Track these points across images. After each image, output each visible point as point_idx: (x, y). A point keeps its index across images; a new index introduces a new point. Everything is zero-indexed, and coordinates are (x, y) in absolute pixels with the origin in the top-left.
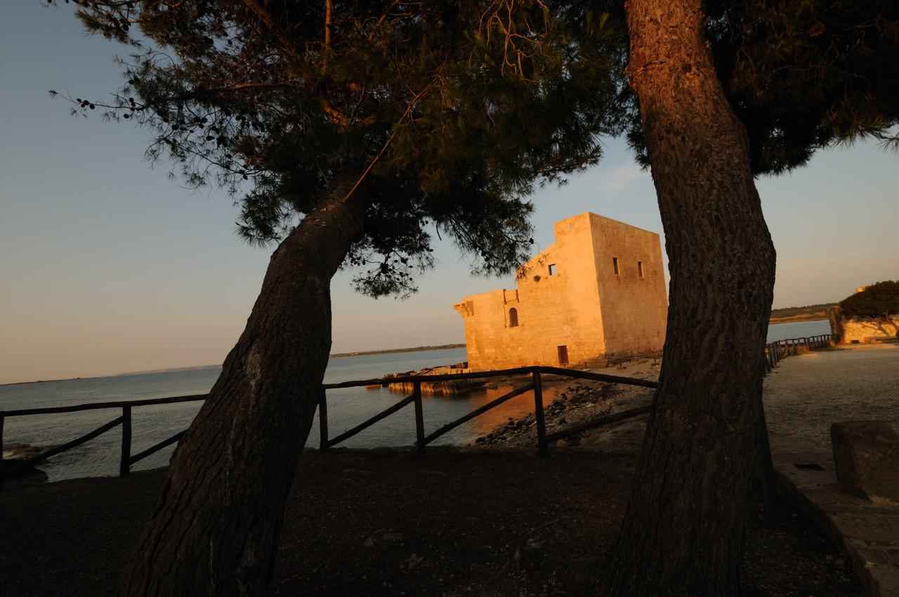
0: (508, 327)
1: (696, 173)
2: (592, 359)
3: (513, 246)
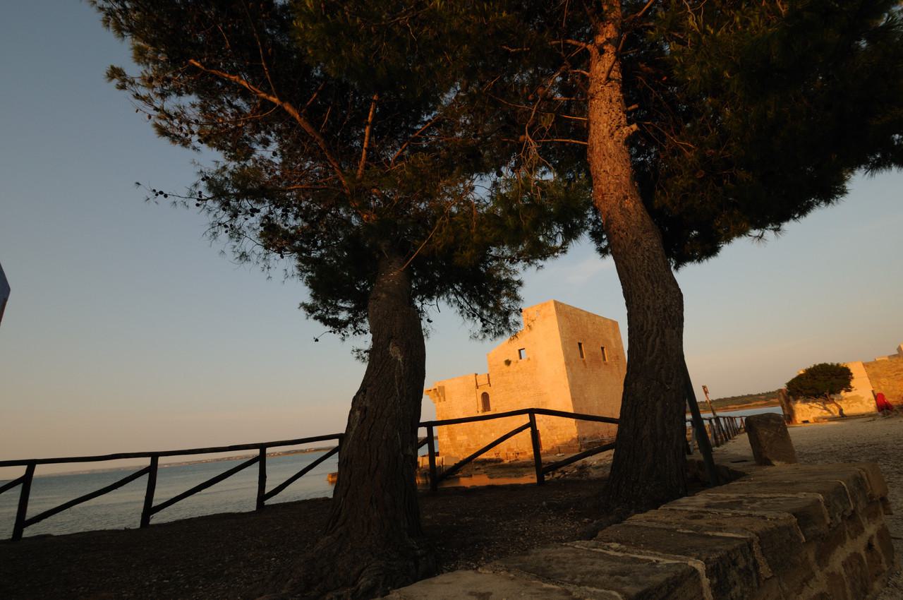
1: (635, 252)
2: (566, 444)
3: (507, 313)
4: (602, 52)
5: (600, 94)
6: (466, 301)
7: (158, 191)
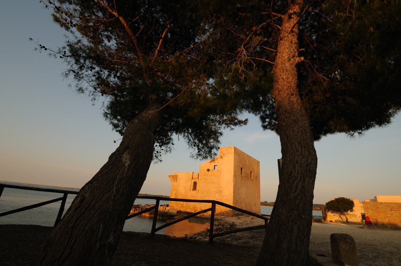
0: (191, 190)
1: (294, 126)
2: (227, 212)
3: (212, 148)
4: (290, 18)
5: (286, 38)
6: (192, 138)
7: (42, 46)
